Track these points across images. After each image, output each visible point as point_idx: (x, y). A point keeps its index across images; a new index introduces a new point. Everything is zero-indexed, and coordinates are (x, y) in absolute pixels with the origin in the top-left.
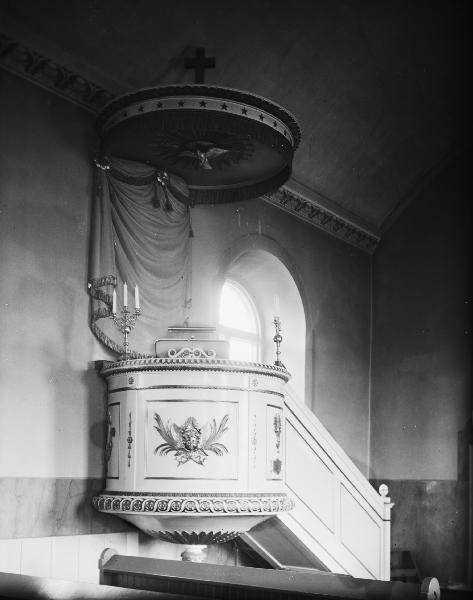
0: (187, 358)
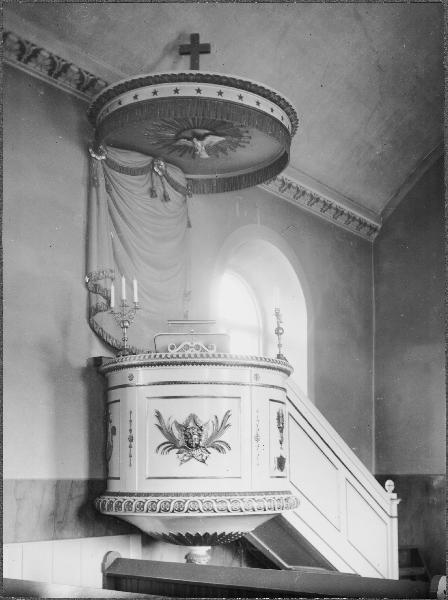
0: (187, 353)
